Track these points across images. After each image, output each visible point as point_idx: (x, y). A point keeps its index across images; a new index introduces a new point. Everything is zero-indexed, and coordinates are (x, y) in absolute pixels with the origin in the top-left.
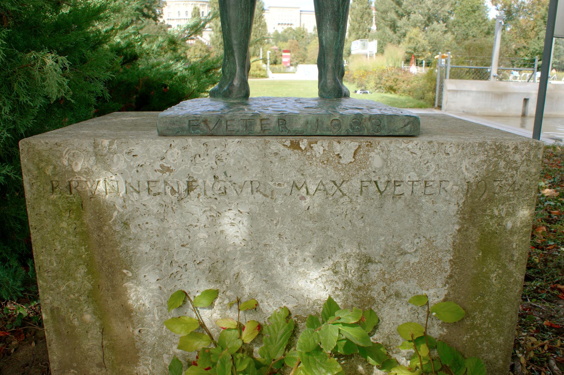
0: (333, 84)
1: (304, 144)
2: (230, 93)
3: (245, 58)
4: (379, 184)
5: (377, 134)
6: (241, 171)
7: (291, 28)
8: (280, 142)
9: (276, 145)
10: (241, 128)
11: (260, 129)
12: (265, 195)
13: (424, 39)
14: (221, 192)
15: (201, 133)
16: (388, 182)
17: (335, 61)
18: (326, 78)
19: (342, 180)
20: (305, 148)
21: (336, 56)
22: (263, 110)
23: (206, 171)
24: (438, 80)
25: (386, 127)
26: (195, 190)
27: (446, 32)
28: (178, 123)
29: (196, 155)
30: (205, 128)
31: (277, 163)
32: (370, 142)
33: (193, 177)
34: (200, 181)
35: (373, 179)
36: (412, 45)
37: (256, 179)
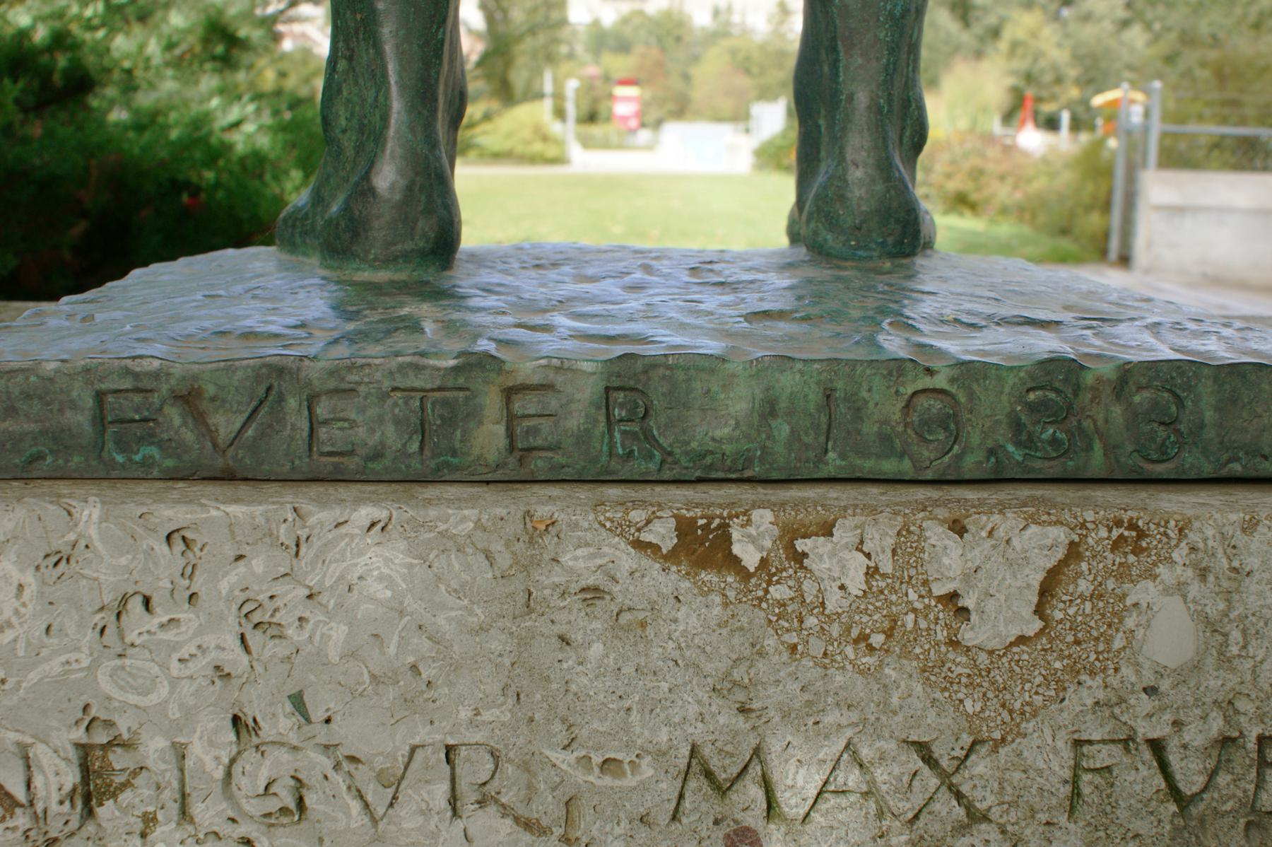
0: (879, 187)
1: (753, 540)
2: (355, 234)
3: (438, 53)
4: (1174, 758)
5: (1161, 469)
6: (391, 692)
7: (641, 13)
8: (619, 529)
9: (592, 540)
10: (391, 436)
11: (502, 442)
12: (527, 825)
13: (1059, 46)
14: (273, 805)
15: (169, 463)
16: (1225, 742)
17: (890, 72)
18: (841, 159)
19: (967, 740)
20: (764, 562)
21: (894, 49)
22: (521, 335)
23: (186, 688)
24: (1120, 173)
25: (1210, 434)
26: (126, 797)
27: (1125, 24)
28: (36, 406)
29: (124, 600)
30: (189, 436)
31: (597, 649)
32: (1132, 526)
33: (109, 724)
34: (154, 747)
35: (1146, 730)
36: (1020, 64)
37: (478, 737)
